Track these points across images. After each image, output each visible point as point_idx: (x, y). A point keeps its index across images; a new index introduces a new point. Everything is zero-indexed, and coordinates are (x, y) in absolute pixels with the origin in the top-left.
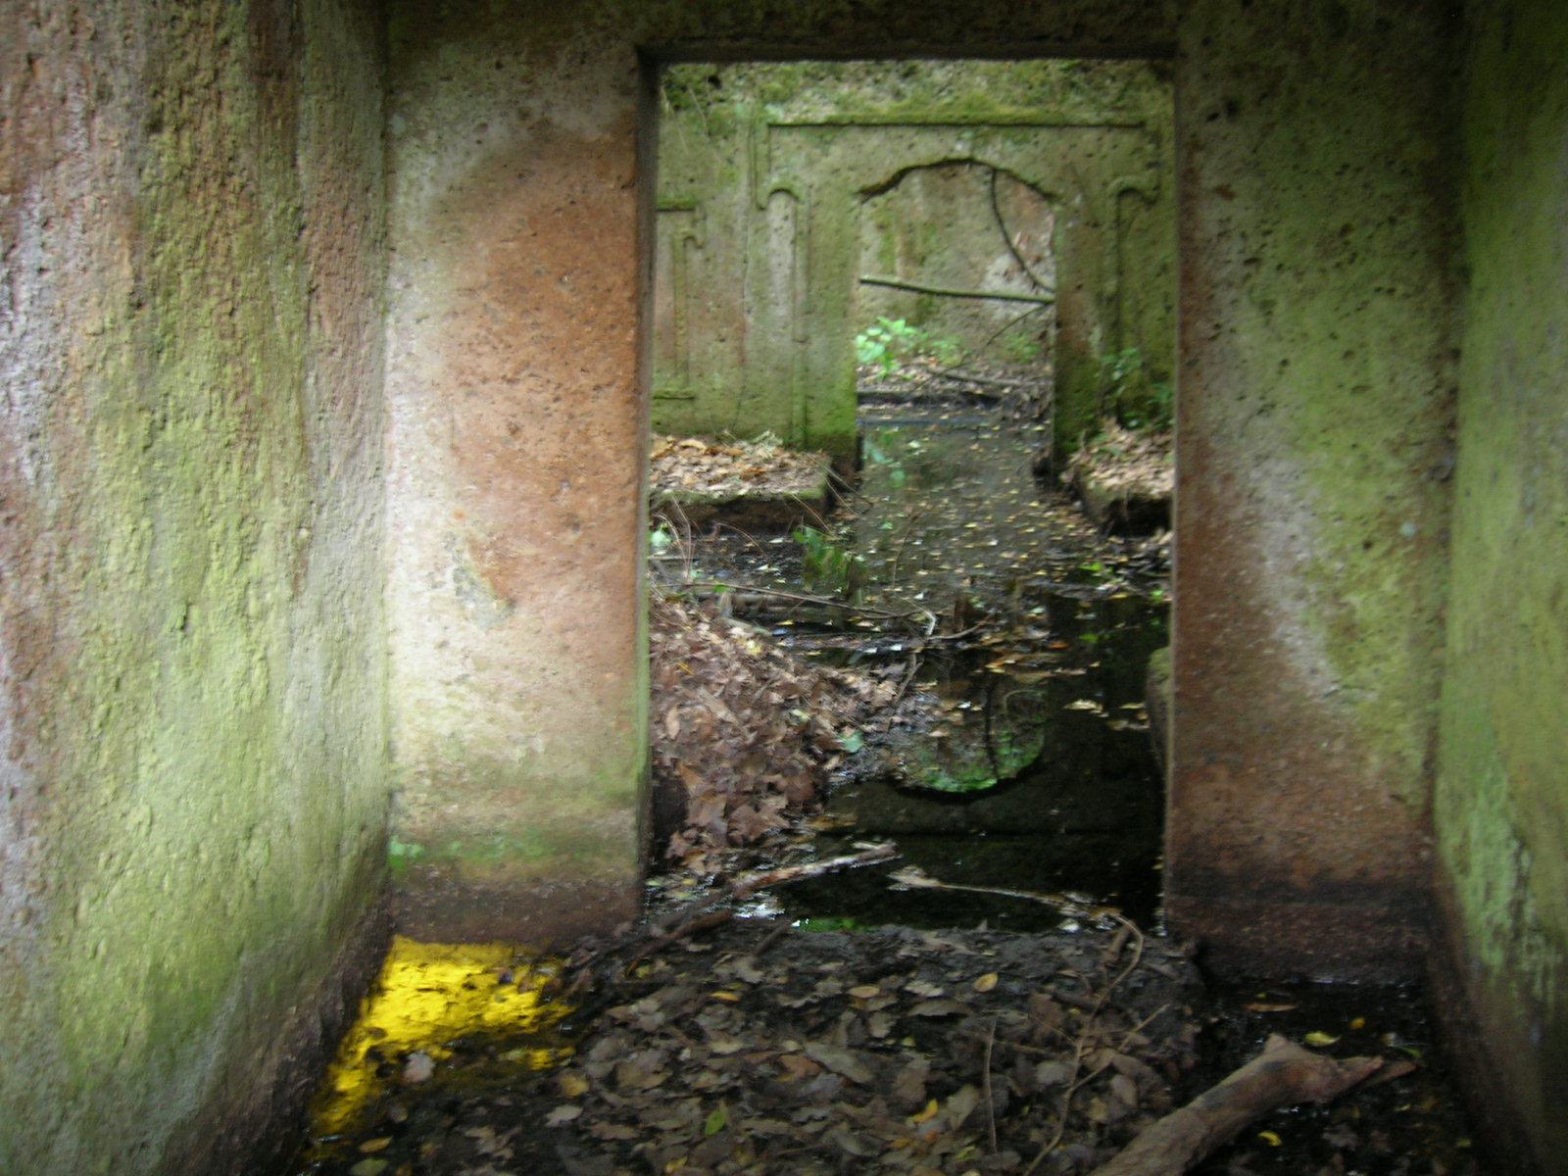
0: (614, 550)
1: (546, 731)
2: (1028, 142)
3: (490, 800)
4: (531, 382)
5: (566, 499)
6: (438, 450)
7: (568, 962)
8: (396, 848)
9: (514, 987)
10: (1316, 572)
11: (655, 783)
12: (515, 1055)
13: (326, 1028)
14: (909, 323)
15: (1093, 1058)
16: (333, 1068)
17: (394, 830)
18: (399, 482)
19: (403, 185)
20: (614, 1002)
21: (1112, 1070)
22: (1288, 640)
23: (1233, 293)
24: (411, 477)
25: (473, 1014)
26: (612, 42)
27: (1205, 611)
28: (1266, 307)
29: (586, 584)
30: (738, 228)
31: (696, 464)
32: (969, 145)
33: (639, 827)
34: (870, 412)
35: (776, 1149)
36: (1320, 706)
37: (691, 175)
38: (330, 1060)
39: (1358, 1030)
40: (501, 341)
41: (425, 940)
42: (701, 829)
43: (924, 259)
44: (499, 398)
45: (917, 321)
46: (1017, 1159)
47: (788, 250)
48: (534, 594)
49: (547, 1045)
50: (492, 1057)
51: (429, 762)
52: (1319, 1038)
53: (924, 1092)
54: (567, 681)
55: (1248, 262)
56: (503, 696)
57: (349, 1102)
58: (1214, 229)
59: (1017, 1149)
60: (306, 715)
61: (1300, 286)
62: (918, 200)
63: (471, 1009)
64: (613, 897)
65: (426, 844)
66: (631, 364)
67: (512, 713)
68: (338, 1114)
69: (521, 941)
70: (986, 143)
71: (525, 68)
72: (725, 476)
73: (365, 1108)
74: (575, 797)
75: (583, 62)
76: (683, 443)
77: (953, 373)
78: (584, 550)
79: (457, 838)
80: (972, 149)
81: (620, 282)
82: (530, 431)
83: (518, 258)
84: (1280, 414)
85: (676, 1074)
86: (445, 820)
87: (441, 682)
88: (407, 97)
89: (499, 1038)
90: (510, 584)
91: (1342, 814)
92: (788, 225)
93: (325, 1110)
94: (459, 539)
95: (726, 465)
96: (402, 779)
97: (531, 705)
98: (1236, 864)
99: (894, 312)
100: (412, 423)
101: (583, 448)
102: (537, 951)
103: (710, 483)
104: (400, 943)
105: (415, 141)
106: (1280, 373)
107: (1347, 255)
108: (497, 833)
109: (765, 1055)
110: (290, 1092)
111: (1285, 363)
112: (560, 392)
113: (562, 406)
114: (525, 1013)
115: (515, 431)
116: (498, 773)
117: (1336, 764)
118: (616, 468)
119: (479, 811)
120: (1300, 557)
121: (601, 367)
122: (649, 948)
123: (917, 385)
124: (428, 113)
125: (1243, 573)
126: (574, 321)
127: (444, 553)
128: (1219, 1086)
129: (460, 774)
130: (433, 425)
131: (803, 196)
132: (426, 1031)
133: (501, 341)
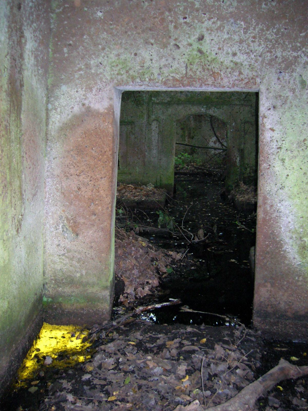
0: (105, 221)
1: (86, 269)
2: (221, 108)
3: (70, 287)
4: (84, 176)
5: (92, 207)
6: (58, 193)
7: (90, 331)
8: (45, 299)
9: (76, 338)
10: (296, 232)
11: (116, 281)
12: (75, 358)
13: (23, 349)
14: (189, 154)
15: (232, 364)
16: (25, 360)
17: (44, 294)
18: (48, 201)
19: (51, 123)
20: (102, 344)
21: (237, 368)
22: (287, 250)
23: (274, 157)
24: (51, 200)
25: (64, 345)
26: (108, 86)
27: (265, 241)
28: (283, 160)
29: (97, 230)
30: (144, 129)
31: (131, 191)
32: (205, 109)
33: (111, 296)
34: (178, 177)
35: (144, 388)
36: (296, 268)
37: (132, 115)
38: (24, 358)
39: (305, 356)
40: (76, 165)
41: (52, 324)
42: (128, 294)
43: (193, 137)
44: (75, 180)
45: (190, 154)
46: (210, 393)
47: (157, 136)
48: (83, 233)
49: (84, 355)
50: (69, 358)
51: (54, 276)
52: (294, 358)
53: (185, 373)
54: (91, 256)
55: (278, 148)
56: (75, 259)
57: (29, 370)
58: (269, 139)
59: (210, 391)
60: (19, 265)
61: (292, 155)
62: (192, 122)
63: (64, 344)
64: (103, 314)
65: (53, 298)
66: (111, 172)
67: (77, 264)
68: (25, 374)
69: (78, 325)
70: (210, 109)
71: (84, 92)
72: (138, 195)
73: (33, 372)
74: (93, 287)
75: (99, 91)
76: (128, 186)
77: (200, 167)
78: (97, 221)
79: (61, 297)
80: (206, 110)
81: (108, 150)
82: (83, 189)
83: (81, 143)
84: (286, 189)
85: (118, 366)
86: (58, 292)
87: (58, 255)
88: (52, 99)
89: (70, 352)
90: (77, 230)
91: (301, 297)
92: (157, 129)
93: (22, 372)
94: (63, 218)
95: (139, 192)
96: (47, 281)
97: (82, 262)
98: (272, 309)
99: (185, 151)
100: (51, 186)
101: (97, 194)
102: (81, 328)
103: (135, 197)
104: (45, 324)
105: (54, 111)
106: (286, 178)
107: (305, 147)
108: (72, 296)
109: (142, 361)
110: (12, 368)
111: (288, 175)
112: (92, 179)
113: (92, 182)
114: (78, 345)
115: (79, 189)
116: (73, 280)
117: (300, 283)
118: (106, 199)
119: (67, 290)
120: (291, 227)
121: (103, 173)
122: (112, 328)
123: (190, 170)
124: (58, 103)
125: (275, 231)
126: (96, 160)
127: (60, 221)
128: (266, 374)
129: (62, 280)
130: (57, 187)
131: (161, 122)
132: (51, 350)
133: (76, 165)
